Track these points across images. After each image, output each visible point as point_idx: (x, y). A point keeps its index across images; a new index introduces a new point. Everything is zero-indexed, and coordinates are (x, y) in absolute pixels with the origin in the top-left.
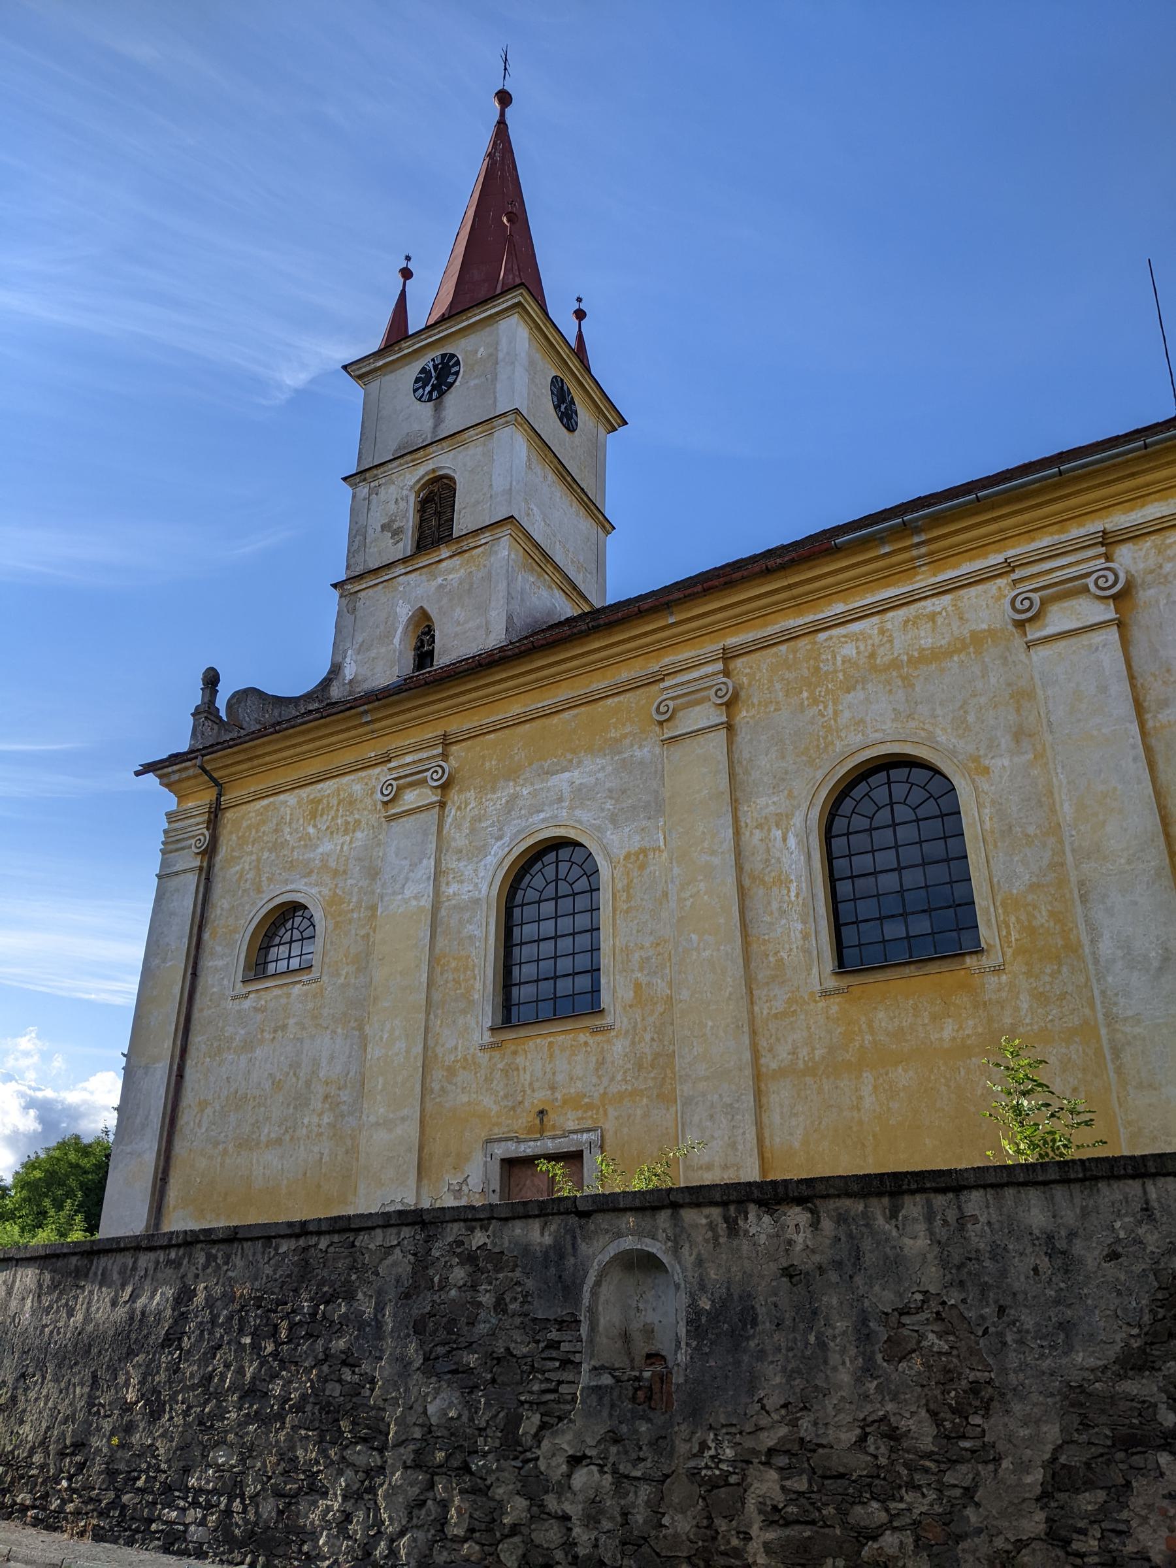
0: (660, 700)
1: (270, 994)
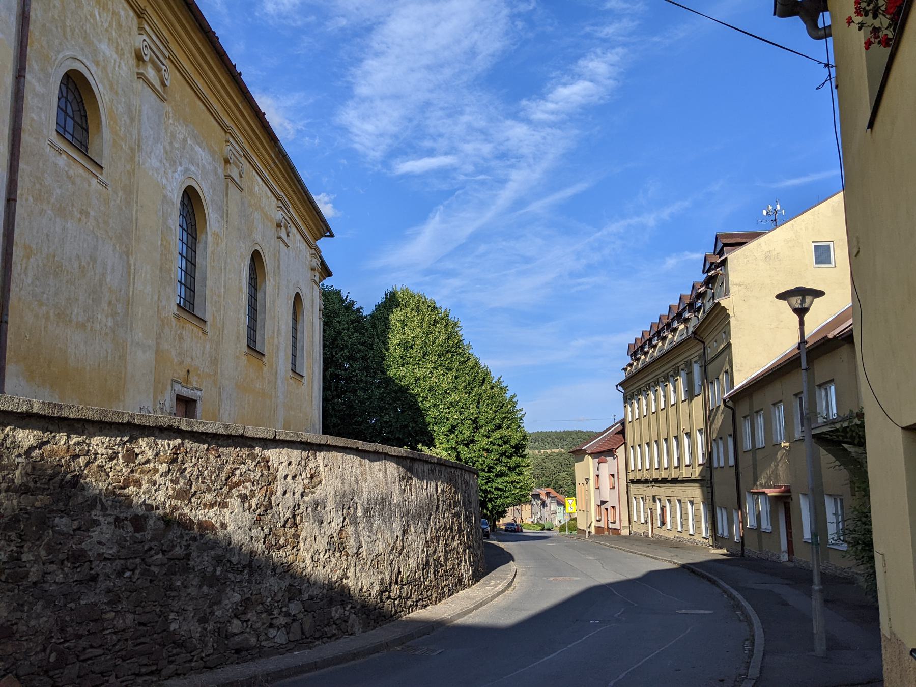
0: (85, 60)
1: (104, 171)
